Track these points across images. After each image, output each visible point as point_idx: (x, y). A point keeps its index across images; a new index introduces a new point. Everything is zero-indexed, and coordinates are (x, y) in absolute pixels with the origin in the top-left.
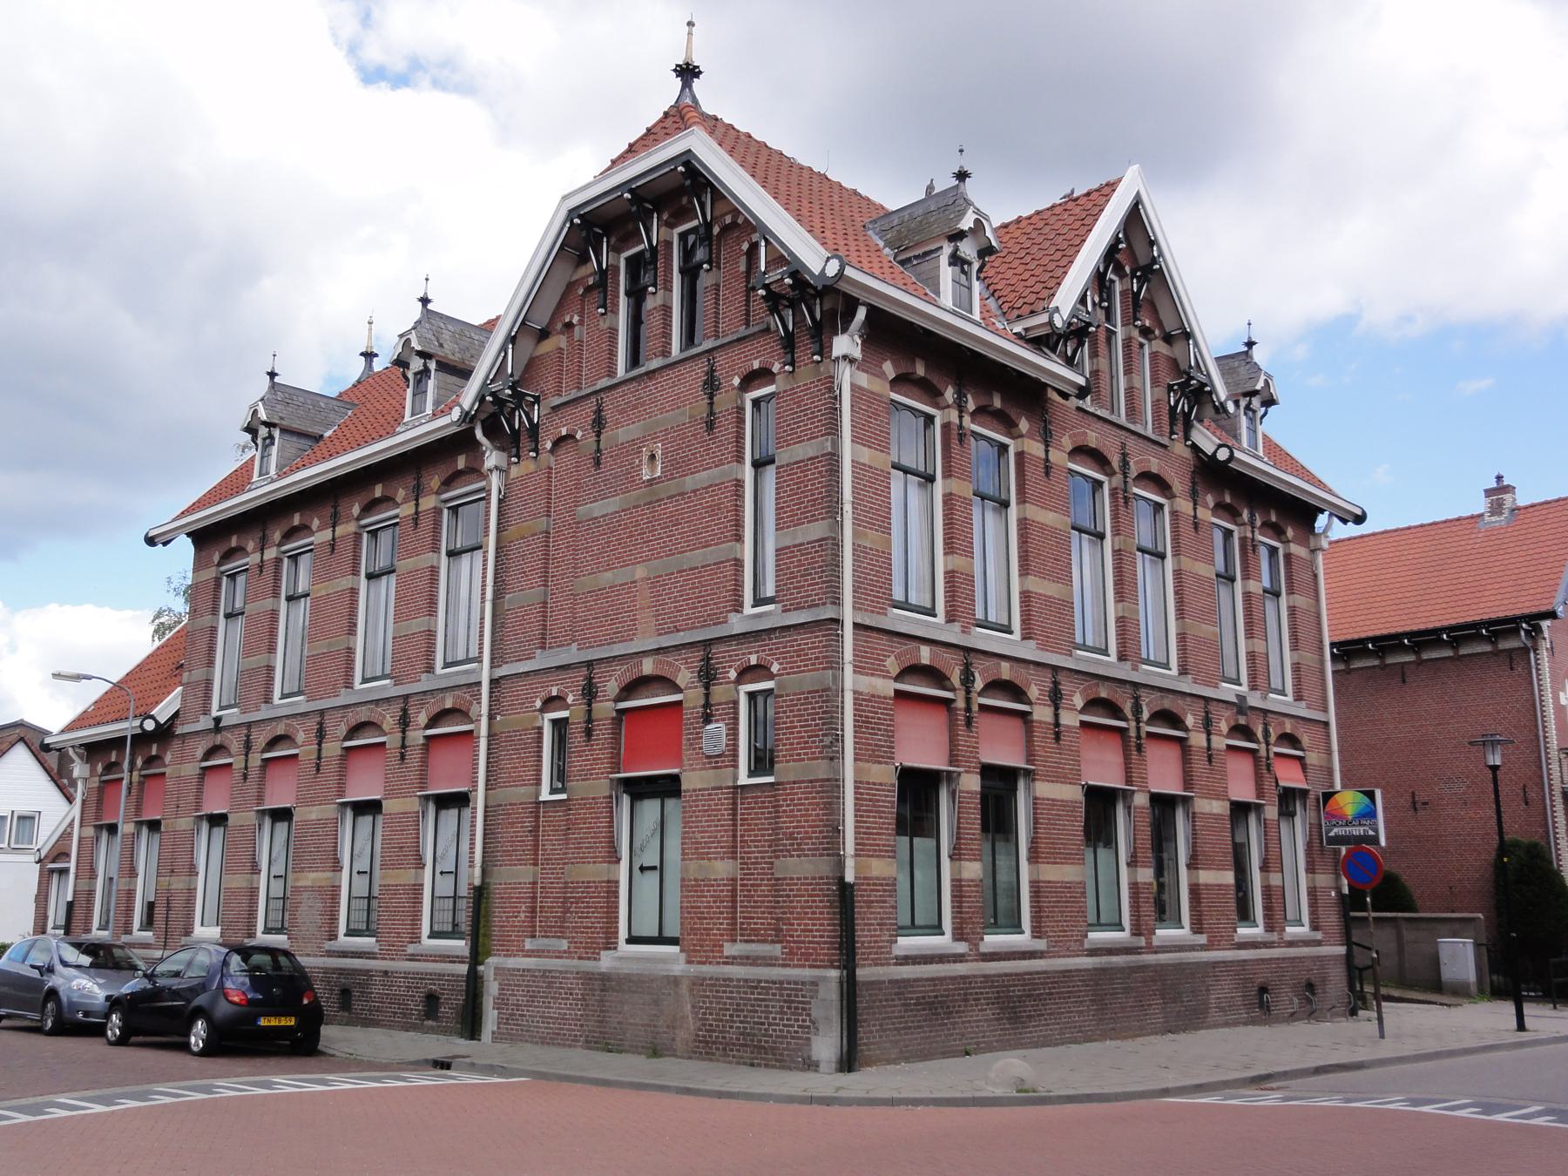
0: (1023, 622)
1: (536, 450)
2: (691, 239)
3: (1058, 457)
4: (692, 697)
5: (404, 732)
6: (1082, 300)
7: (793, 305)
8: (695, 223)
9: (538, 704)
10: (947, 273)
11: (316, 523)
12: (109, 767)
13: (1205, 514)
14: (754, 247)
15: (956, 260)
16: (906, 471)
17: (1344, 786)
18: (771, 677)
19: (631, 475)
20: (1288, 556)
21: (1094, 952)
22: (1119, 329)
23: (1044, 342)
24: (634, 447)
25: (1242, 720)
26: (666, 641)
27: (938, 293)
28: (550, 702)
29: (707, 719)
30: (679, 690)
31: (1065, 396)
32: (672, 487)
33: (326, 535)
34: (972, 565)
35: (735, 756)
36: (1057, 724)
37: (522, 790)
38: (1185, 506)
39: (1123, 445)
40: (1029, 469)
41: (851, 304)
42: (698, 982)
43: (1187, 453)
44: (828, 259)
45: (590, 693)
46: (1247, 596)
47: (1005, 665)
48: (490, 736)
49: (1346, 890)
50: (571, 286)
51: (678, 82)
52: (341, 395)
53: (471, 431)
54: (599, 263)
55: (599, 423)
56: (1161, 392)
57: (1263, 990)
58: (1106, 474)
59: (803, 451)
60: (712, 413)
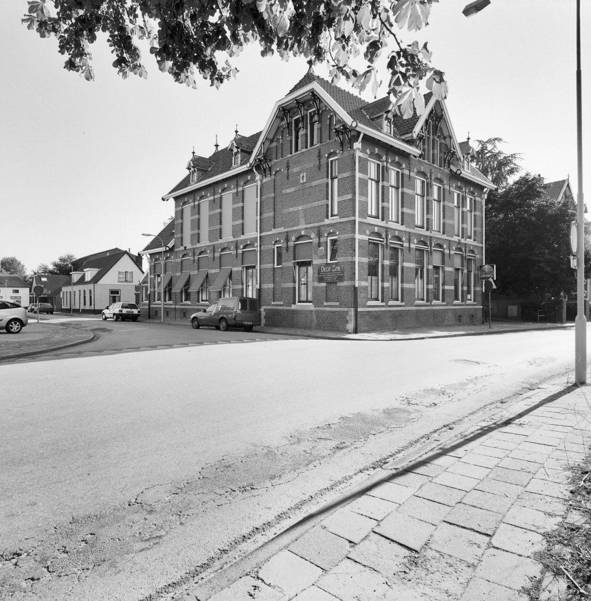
0: (402, 220)
1: (270, 175)
2: (312, 114)
3: (412, 174)
4: (316, 241)
5: (237, 250)
6: (422, 129)
7: (342, 134)
8: (314, 109)
9: (273, 243)
10: (385, 123)
11: (209, 194)
12: (156, 260)
13: (452, 189)
14: (331, 116)
15: (387, 118)
16: (372, 180)
17: (485, 264)
18: (336, 235)
19: (297, 182)
20: (475, 201)
21: (417, 306)
22: (431, 137)
23: (410, 142)
24: (299, 173)
25: (459, 246)
26: (308, 226)
27: (382, 129)
28: (276, 242)
29: (319, 246)
30: (311, 239)
31: (415, 157)
32: (308, 185)
33: (212, 198)
34: (389, 205)
35: (327, 255)
36: (410, 247)
37: (269, 265)
38: (447, 187)
39: (431, 170)
40: (405, 178)
41: (359, 133)
42: (317, 312)
43: (448, 172)
44: (353, 122)
45: (287, 240)
46: (463, 212)
47: (397, 232)
48: (260, 251)
49: (484, 291)
50: (279, 128)
51: (308, 66)
52: (210, 157)
53: (252, 169)
54: (287, 120)
55: (288, 167)
56: (442, 154)
57: (460, 316)
58: (425, 178)
59: (346, 175)
60: (320, 164)
